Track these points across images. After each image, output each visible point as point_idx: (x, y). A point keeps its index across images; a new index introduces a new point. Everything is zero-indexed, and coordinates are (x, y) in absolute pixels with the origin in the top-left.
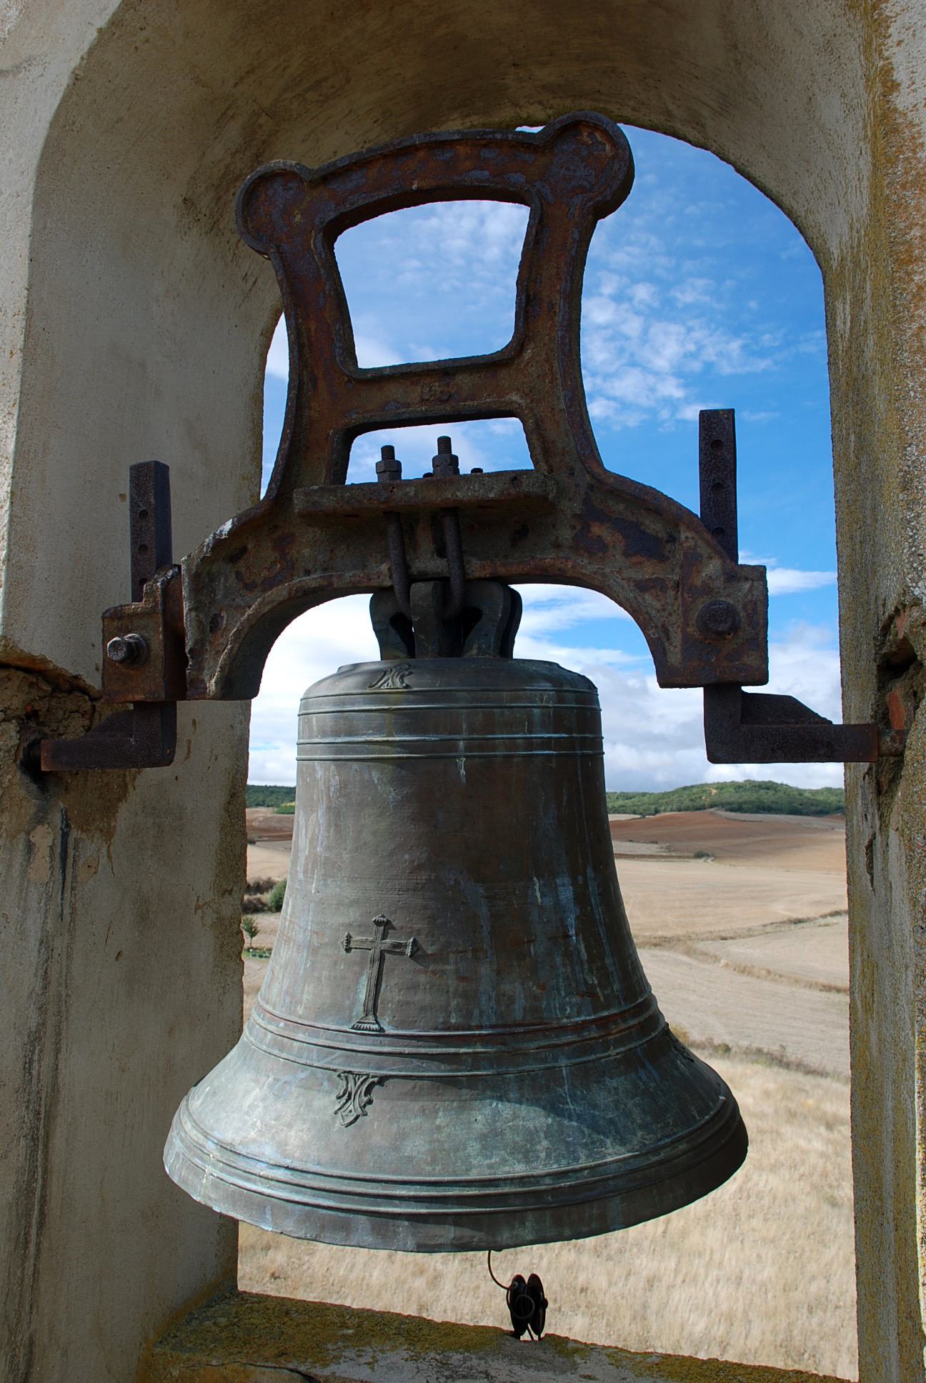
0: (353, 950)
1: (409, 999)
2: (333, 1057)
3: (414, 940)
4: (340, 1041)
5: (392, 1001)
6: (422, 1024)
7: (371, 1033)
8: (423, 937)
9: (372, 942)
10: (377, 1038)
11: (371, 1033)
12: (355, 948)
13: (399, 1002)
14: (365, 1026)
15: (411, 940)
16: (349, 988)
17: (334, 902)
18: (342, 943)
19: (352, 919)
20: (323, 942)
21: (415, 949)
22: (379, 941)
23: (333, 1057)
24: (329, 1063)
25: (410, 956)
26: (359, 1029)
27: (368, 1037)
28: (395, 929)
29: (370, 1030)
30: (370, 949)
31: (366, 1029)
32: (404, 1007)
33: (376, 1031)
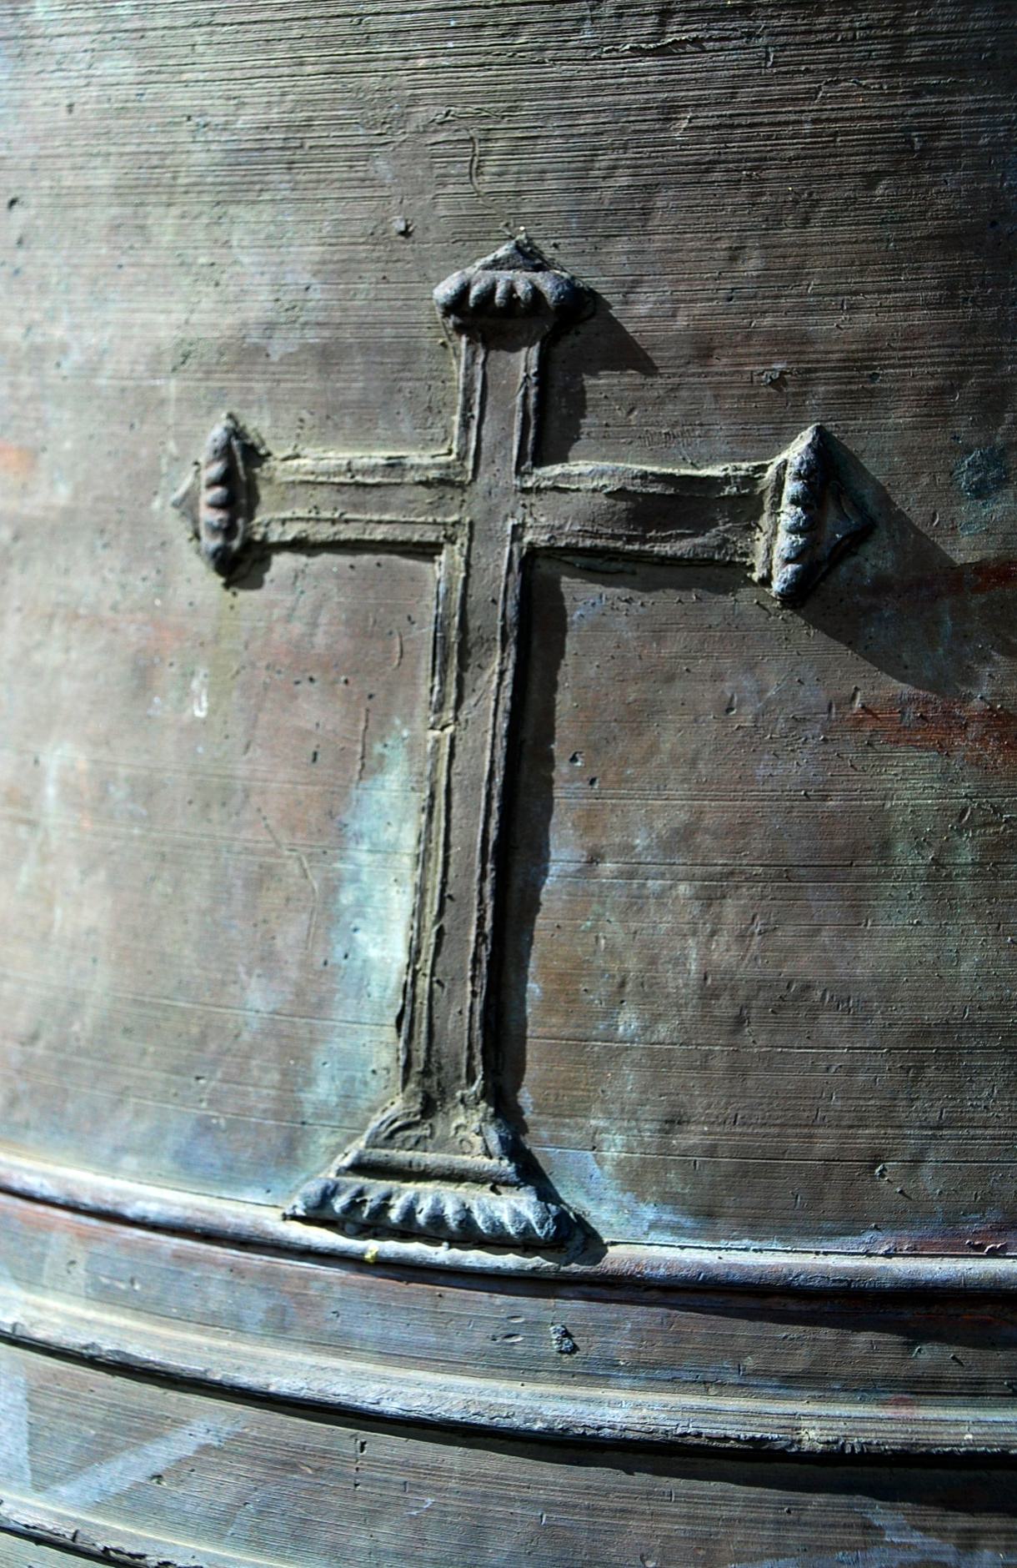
0: (282, 562)
1: (803, 966)
2: (160, 1454)
3: (824, 447)
4: (210, 1321)
5: (649, 990)
6: (928, 1181)
7: (475, 1258)
8: (900, 416)
9: (445, 483)
10: (529, 1306)
11: (475, 1258)
12: (299, 545)
13: (708, 993)
14: (428, 1197)
15: (796, 451)
16: (262, 877)
17: (103, 177)
18: (187, 506)
19: (259, 306)
20: (31, 507)
21: (835, 530)
22: (500, 473)
23: (160, 1454)
24: (132, 1503)
25: (795, 596)
26: (376, 1226)
27: (453, 1294)
28: (647, 367)
29: (467, 1234)
30: (427, 551)
31: (435, 1230)
32: (755, 1039)
33: (525, 1243)
